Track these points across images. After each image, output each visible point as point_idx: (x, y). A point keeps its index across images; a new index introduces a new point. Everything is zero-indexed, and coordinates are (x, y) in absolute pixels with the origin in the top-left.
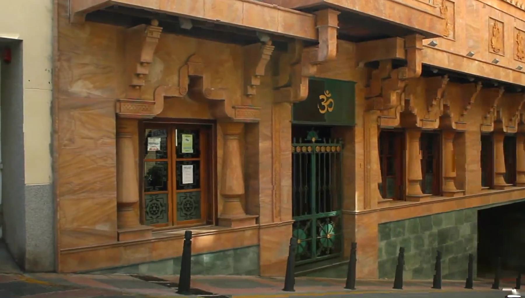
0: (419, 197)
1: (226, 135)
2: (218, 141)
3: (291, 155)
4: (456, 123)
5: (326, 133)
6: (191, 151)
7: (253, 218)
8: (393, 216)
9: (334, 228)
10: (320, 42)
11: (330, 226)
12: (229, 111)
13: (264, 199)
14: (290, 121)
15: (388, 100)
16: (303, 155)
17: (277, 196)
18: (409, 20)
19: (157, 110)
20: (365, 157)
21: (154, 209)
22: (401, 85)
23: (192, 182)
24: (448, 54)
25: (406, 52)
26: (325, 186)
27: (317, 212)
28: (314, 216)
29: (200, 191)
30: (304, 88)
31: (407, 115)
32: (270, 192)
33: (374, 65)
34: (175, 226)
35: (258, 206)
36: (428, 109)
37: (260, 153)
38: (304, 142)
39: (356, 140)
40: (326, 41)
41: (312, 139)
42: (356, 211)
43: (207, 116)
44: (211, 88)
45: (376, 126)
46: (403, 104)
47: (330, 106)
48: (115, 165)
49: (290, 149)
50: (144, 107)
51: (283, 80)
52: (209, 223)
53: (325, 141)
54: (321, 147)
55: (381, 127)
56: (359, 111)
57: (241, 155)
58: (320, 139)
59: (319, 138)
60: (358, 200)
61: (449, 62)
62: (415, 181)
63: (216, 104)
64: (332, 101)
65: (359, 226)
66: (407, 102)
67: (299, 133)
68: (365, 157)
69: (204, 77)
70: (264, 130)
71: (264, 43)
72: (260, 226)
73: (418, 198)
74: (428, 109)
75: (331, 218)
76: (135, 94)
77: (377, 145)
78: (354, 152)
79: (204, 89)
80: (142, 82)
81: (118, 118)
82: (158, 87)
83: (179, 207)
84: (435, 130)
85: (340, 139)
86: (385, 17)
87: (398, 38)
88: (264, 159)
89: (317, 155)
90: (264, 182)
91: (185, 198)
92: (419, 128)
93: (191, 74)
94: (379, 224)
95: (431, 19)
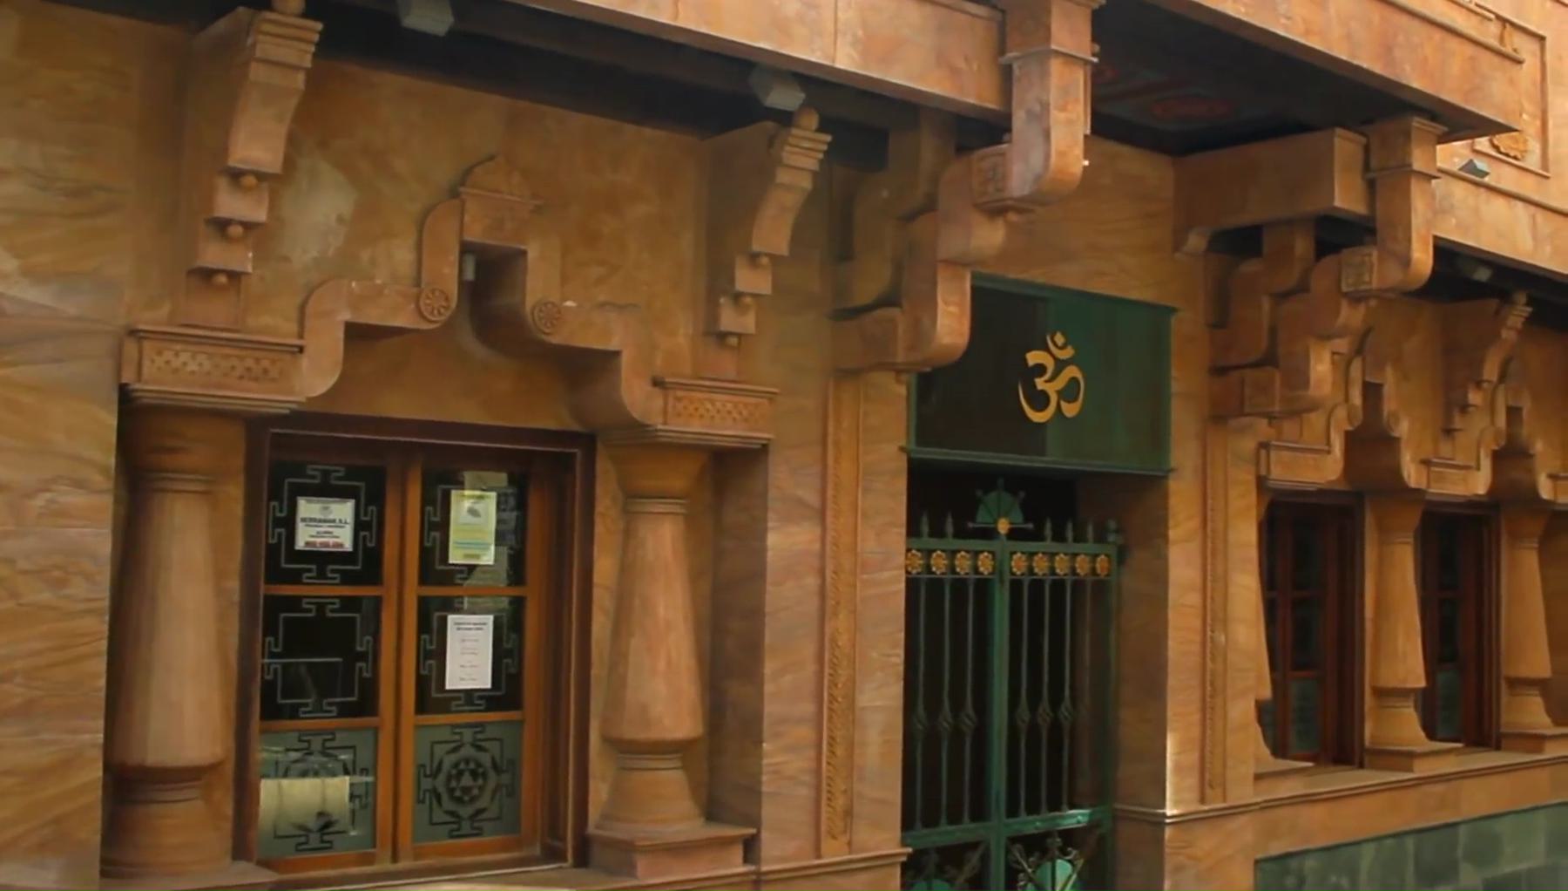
0: (1411, 755)
1: (632, 496)
2: (598, 520)
3: (902, 586)
4: (1553, 477)
5: (1054, 503)
6: (300, 544)
7: (725, 843)
8: (1316, 827)
9: (1079, 875)
10: (1019, 120)
11: (1063, 869)
12: (636, 396)
13: (783, 760)
14: (902, 449)
15: (1299, 377)
16: (959, 585)
17: (840, 751)
18: (1387, 50)
19: (314, 378)
20: (1208, 597)
21: (467, 780)
22: (1351, 316)
23: (489, 686)
24: (1532, 209)
25: (1371, 185)
26: (1045, 705)
27: (1012, 811)
28: (998, 830)
29: (521, 723)
30: (952, 309)
31: (1371, 441)
32: (805, 733)
33: (1241, 243)
34: (403, 865)
35: (753, 792)
36: (1448, 417)
37: (770, 577)
38: (961, 533)
39: (1173, 534)
40: (1041, 117)
41: (996, 522)
42: (1169, 812)
43: (551, 416)
44: (558, 294)
45: (1252, 478)
46: (1357, 398)
47: (1069, 393)
48: (106, 603)
49: (901, 560)
50: (250, 363)
51: (869, 283)
52: (553, 854)
53: (1048, 531)
54: (1031, 555)
55: (1271, 484)
56: (1183, 420)
57: (694, 577)
58: (1030, 526)
59: (1026, 520)
60: (1178, 769)
61: (1535, 238)
62: (1403, 693)
63: (585, 368)
64: (1079, 375)
65: (1179, 869)
66: (1372, 392)
67: (938, 499)
68: (1208, 597)
69: (533, 252)
70: (786, 479)
71: (785, 119)
72: (758, 873)
73: (1404, 758)
74: (1448, 417)
75: (1070, 838)
76: (214, 310)
77: (1253, 553)
78: (1160, 579)
79: (530, 301)
80: (241, 259)
81: (130, 408)
82: (321, 284)
83: (427, 783)
84: (1472, 503)
85: (1112, 525)
86: (1286, 28)
87: (1339, 131)
88: (787, 599)
89: (1016, 585)
90: (784, 689)
91: (455, 750)
92: (1417, 490)
93: (475, 234)
94: (1257, 862)
95: (1472, 58)
